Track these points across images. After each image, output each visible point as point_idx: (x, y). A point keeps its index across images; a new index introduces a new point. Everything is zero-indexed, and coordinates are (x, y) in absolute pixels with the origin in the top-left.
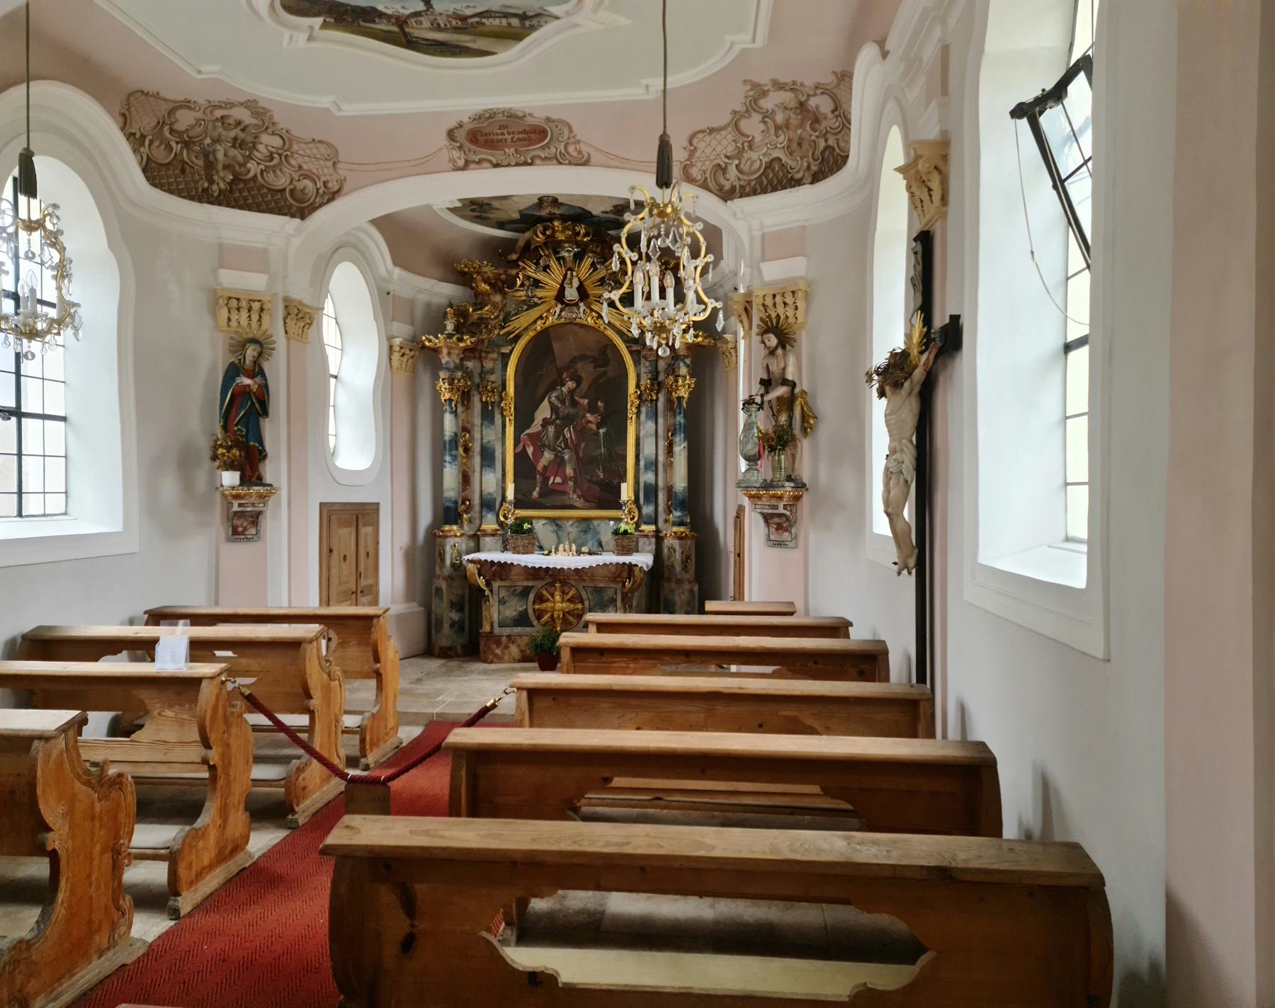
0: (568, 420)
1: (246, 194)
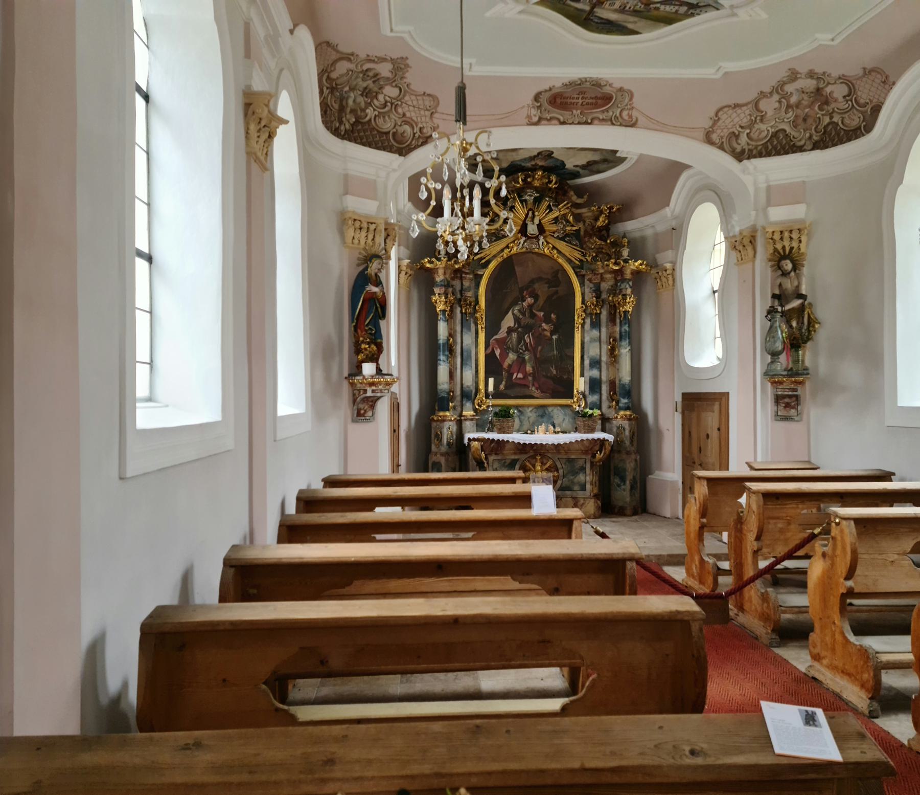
0: (528, 329)
1: (362, 134)
